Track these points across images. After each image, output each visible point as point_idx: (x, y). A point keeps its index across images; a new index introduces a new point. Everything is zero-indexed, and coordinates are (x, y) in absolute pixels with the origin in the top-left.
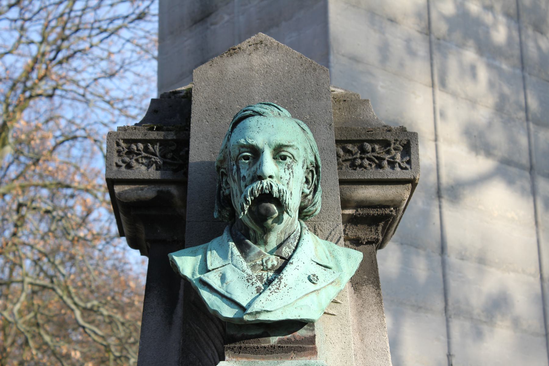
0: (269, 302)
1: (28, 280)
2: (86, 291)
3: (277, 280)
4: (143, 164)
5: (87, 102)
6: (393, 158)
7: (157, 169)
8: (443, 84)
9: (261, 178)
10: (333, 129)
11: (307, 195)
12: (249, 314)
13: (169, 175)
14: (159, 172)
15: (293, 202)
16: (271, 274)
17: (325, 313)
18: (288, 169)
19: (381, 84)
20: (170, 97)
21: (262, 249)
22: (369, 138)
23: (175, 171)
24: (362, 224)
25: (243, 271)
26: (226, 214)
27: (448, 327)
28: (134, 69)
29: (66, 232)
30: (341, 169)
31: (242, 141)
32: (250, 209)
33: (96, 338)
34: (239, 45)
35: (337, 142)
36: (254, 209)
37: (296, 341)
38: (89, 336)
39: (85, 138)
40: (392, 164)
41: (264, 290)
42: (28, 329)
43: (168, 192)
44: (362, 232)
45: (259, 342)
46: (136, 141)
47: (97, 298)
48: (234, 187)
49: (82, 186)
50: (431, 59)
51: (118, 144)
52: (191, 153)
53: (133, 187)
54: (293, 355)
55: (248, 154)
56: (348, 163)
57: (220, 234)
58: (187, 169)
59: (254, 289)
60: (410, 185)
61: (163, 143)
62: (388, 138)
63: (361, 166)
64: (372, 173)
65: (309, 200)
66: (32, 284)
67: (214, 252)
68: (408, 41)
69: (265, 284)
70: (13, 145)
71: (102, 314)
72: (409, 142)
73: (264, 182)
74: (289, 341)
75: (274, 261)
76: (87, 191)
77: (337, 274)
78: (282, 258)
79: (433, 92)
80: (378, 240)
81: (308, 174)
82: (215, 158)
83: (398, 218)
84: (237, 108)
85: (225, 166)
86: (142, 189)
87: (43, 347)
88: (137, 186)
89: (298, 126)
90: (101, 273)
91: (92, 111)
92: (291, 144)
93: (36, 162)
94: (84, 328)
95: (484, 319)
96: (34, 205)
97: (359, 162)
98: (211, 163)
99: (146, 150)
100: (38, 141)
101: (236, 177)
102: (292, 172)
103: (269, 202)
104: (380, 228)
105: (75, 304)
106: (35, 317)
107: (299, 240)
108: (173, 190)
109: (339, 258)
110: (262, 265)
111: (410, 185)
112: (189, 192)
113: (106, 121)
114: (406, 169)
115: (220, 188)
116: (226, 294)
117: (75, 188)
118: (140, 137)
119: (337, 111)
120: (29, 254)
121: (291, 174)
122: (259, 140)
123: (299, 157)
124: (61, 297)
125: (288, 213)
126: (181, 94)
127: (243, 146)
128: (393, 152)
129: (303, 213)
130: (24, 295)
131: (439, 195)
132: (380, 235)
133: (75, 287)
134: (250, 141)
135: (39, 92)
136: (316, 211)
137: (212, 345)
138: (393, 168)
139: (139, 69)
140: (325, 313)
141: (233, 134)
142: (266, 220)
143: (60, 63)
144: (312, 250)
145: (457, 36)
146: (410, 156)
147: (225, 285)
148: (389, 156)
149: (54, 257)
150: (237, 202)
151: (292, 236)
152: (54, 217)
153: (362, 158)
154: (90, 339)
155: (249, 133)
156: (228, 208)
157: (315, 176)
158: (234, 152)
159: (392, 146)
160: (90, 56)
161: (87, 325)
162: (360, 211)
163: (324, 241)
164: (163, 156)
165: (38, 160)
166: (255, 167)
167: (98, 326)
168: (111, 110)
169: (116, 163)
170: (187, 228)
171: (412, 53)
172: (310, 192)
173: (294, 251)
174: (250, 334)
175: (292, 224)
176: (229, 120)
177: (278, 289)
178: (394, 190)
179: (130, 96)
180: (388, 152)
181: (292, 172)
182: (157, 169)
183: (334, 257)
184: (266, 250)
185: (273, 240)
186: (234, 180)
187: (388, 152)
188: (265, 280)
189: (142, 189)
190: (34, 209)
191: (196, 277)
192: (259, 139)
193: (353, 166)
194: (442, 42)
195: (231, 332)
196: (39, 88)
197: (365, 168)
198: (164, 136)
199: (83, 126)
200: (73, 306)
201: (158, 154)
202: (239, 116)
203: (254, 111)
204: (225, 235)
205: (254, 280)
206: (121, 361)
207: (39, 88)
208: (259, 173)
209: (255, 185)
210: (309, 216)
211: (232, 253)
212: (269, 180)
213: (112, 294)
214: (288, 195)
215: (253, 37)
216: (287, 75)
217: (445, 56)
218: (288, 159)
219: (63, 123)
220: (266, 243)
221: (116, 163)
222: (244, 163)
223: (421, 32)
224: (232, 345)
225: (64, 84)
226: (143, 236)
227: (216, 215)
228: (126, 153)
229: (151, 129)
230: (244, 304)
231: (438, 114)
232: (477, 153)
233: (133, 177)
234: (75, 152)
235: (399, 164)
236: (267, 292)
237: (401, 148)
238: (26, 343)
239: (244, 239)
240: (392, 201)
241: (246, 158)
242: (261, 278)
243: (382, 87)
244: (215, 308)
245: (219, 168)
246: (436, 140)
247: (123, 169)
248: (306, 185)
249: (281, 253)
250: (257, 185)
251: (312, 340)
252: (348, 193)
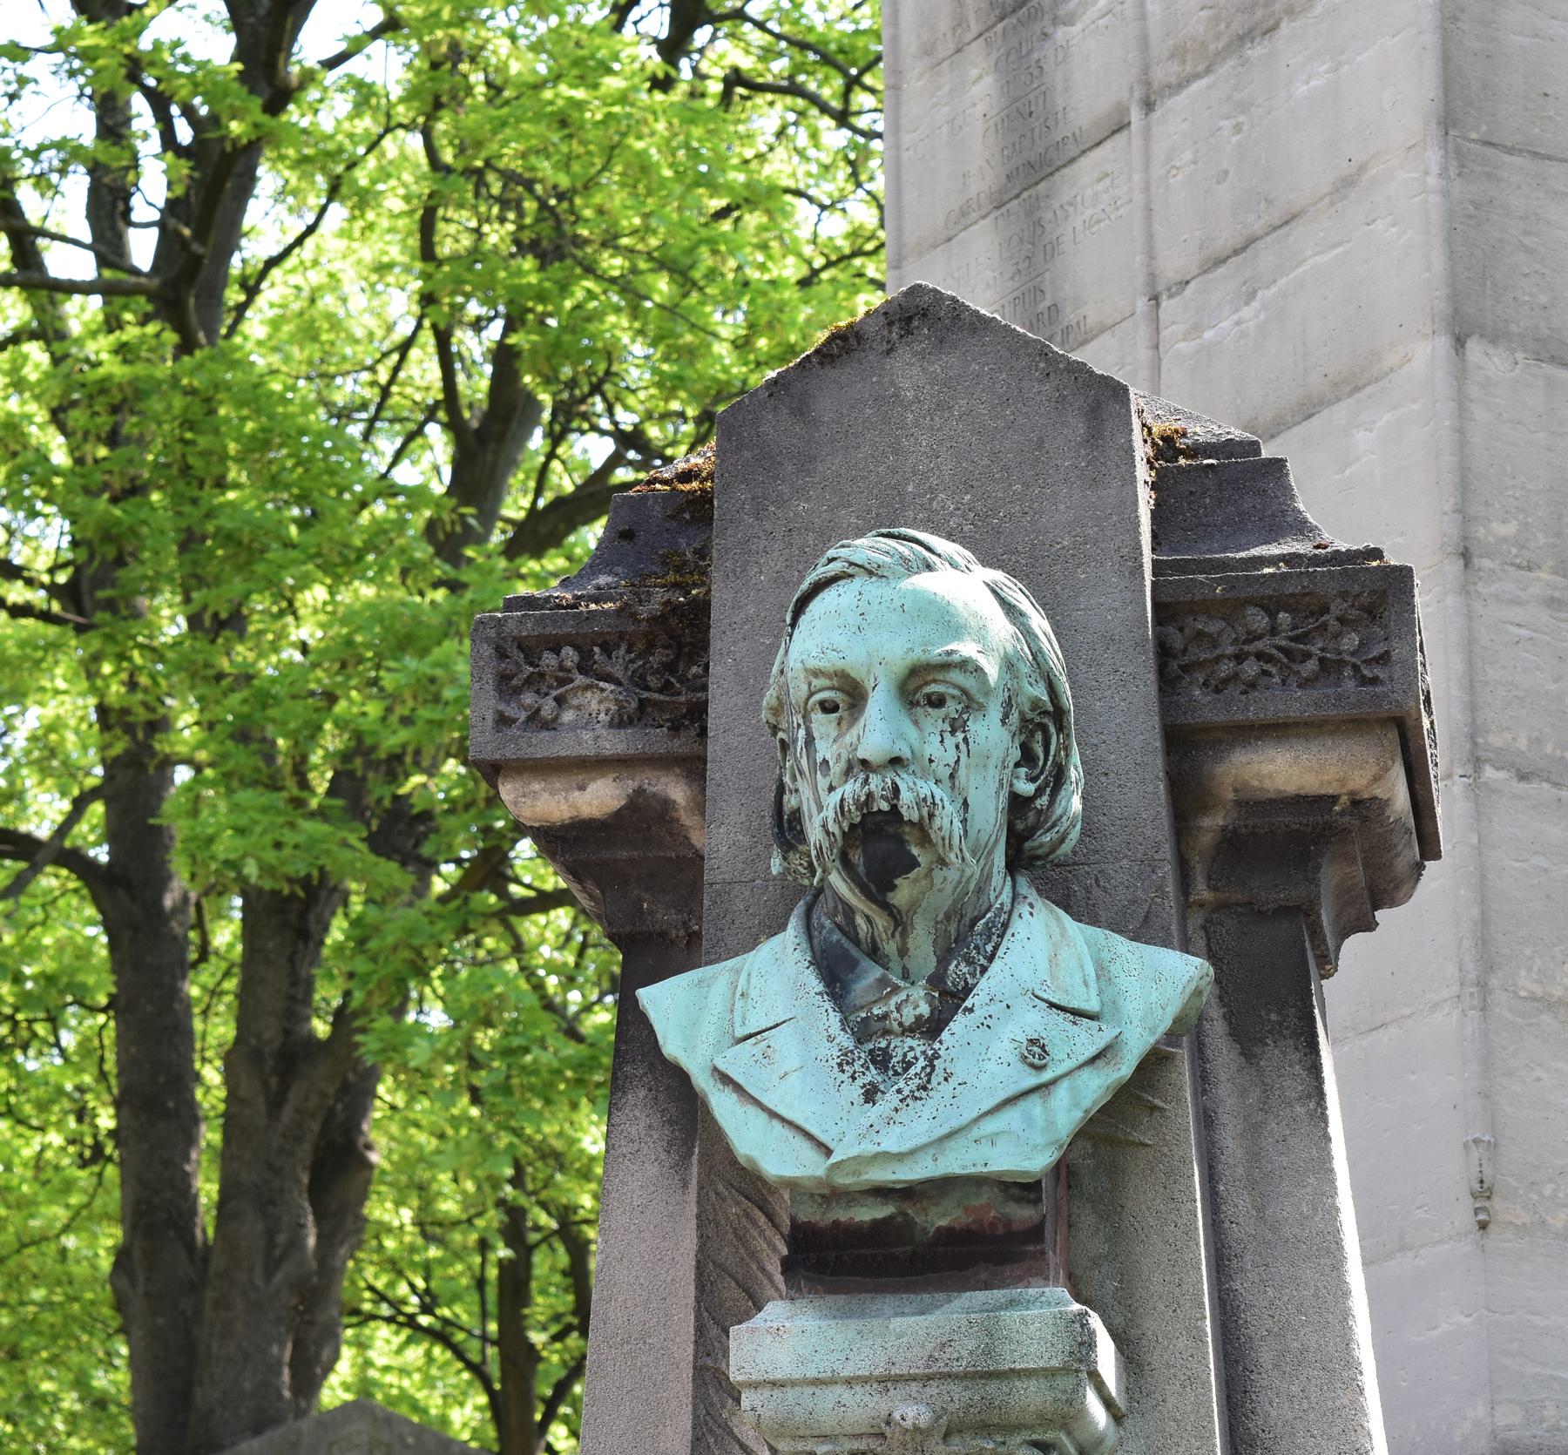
18: (953, 732)
65: (1040, 812)
70: (251, 585)
81: (1032, 734)
102: (965, 740)
108: (677, 791)
115: (781, 789)
121: (963, 747)
136: (1062, 840)
166: (854, 732)
175: (980, 890)
177: (925, 1088)
181: (965, 740)
205: (857, 1066)
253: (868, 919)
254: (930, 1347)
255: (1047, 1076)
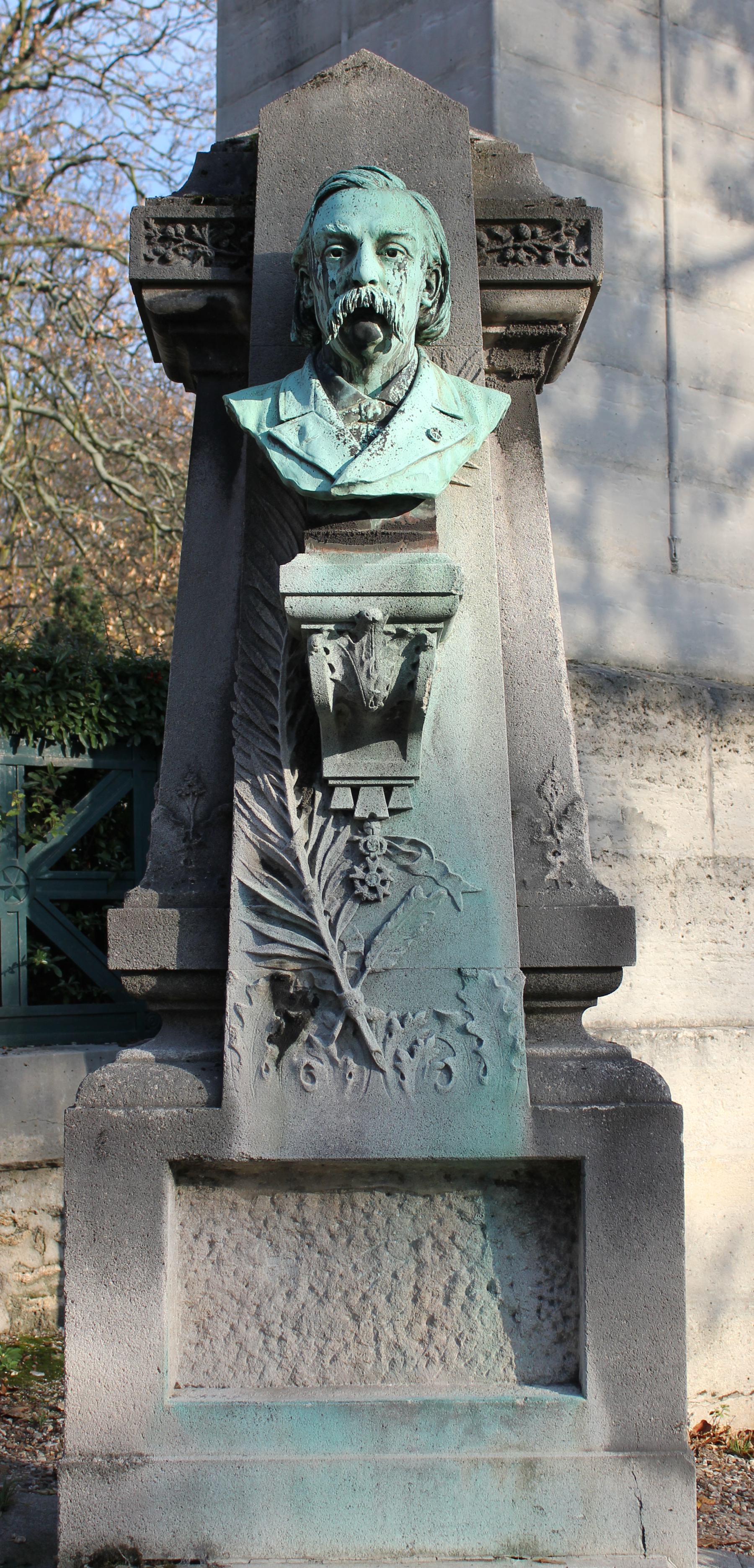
0: (368, 469)
1: (15, 404)
2: (111, 422)
3: (380, 437)
4: (185, 256)
5: (106, 95)
6: (564, 247)
7: (206, 265)
8: (679, 101)
9: (358, 284)
10: (473, 202)
11: (428, 308)
12: (341, 486)
13: (224, 274)
14: (209, 269)
15: (406, 320)
16: (372, 427)
17: (452, 483)
18: (399, 270)
19: (577, 101)
20: (225, 150)
21: (360, 390)
22: (529, 216)
23: (233, 268)
24: (516, 348)
25: (332, 423)
26: (308, 336)
27: (672, 495)
28: (185, 35)
29: (75, 324)
30: (485, 264)
31: (331, 227)
32: (341, 331)
33: (130, 501)
34: (331, 69)
35: (479, 222)
36: (347, 330)
37: (408, 526)
38: (119, 496)
39: (104, 159)
40: (562, 257)
41: (361, 451)
42: (18, 484)
43: (224, 300)
44: (516, 361)
45: (354, 527)
46: (174, 221)
47: (129, 435)
48: (319, 296)
49: (101, 245)
50: (662, 58)
51: (147, 226)
52: (257, 239)
53: (170, 291)
54: (403, 545)
55: (339, 247)
56: (495, 256)
57: (300, 366)
58: (252, 265)
59: (347, 451)
60: (588, 290)
61: (216, 224)
62: (557, 217)
63: (515, 260)
64: (531, 271)
66: (23, 411)
67: (290, 394)
68: (625, 26)
69: (364, 442)
71: (138, 461)
72: (588, 223)
73: (363, 290)
74: (397, 525)
75: (377, 408)
76: (109, 252)
77: (470, 428)
78: (388, 403)
79: (663, 114)
80: (539, 372)
81: (431, 275)
82: (294, 249)
83: (573, 339)
84: (327, 171)
85: (306, 264)
86: (184, 295)
87: (44, 514)
88: (177, 290)
89: (415, 203)
90: (134, 394)
91: (115, 114)
92: (404, 232)
93: (22, 202)
94: (109, 483)
95: (729, 483)
96: (21, 278)
97: (511, 253)
98: (287, 257)
99: (189, 234)
100: (24, 167)
101: (321, 282)
103: (368, 322)
104: (543, 354)
105: (95, 444)
106: (30, 463)
107: (415, 376)
108: (231, 296)
109: (474, 403)
110: (360, 413)
111: (588, 290)
112: (253, 300)
113: (138, 130)
114: (582, 264)
115: (299, 296)
116: (306, 457)
117: (88, 248)
118: (180, 215)
119: (482, 173)
120: (15, 360)
122: (355, 226)
123: (416, 252)
124: (71, 433)
125: (397, 336)
126: (243, 145)
127: (331, 235)
128: (564, 238)
129: (422, 335)
130: (10, 429)
131: (666, 285)
132: (543, 366)
133: (94, 416)
134: (342, 228)
135: (23, 79)
137: (288, 529)
138: (563, 263)
139: (193, 35)
140: (452, 483)
141: (317, 215)
142: (366, 347)
143: (59, 26)
144: (434, 389)
145: (706, 18)
146: (589, 245)
147: (304, 443)
148: (557, 245)
149: (57, 366)
150: (323, 318)
151: (404, 371)
152: (55, 299)
153: (516, 248)
154: (119, 500)
155: (342, 215)
156: (312, 328)
157: (441, 279)
158: (319, 244)
159: (563, 228)
160: (109, 13)
161: (114, 479)
162: (513, 329)
163: (454, 377)
164: (215, 244)
165: (25, 199)
166: (349, 267)
167: (132, 480)
168: (147, 110)
169: (145, 256)
170: (251, 356)
171: (629, 47)
172: (433, 304)
173: (408, 393)
174: (340, 515)
175: (404, 352)
176: (314, 188)
178: (564, 297)
179: (180, 85)
180: (557, 239)
182: (206, 265)
183: (467, 402)
184: (366, 391)
185: (377, 376)
186: (319, 287)
187: (557, 239)
188: (363, 435)
189: (184, 295)
190: (22, 284)
191: (262, 431)
192: (355, 224)
193: (503, 260)
194: (681, 28)
195: (314, 512)
196: (23, 72)
197: (521, 263)
198: (216, 213)
199: (100, 139)
200: (91, 448)
201: (207, 240)
202: (327, 187)
203: (348, 181)
204: (306, 369)
205: (346, 436)
206: (171, 538)
207: (23, 72)
208: (354, 277)
209: (348, 295)
210: (432, 339)
211: (316, 395)
212: (369, 287)
213: (156, 428)
214: (399, 308)
215: (352, 57)
216: (403, 117)
217: (683, 52)
218: (399, 255)
219: (65, 132)
220: (365, 381)
221: (145, 256)
222: (333, 261)
223: (645, 13)
224: (315, 531)
225: (64, 65)
226: (187, 365)
227: (293, 337)
228: (160, 240)
229: (197, 202)
230: (332, 472)
231: (668, 151)
232: (732, 217)
233: (170, 277)
234: (86, 183)
235: (573, 257)
236: (366, 454)
237: (577, 232)
238: (17, 507)
239: (333, 376)
240: (561, 314)
241: (337, 253)
242: (357, 434)
243: (577, 106)
244: (291, 478)
245: (297, 267)
246: (665, 195)
247: (155, 264)
248: (427, 293)
249: (387, 396)
250: (352, 295)
251: (431, 524)
252: (494, 302)
253: (349, 364)
254: (381, 579)
255: (439, 447)
